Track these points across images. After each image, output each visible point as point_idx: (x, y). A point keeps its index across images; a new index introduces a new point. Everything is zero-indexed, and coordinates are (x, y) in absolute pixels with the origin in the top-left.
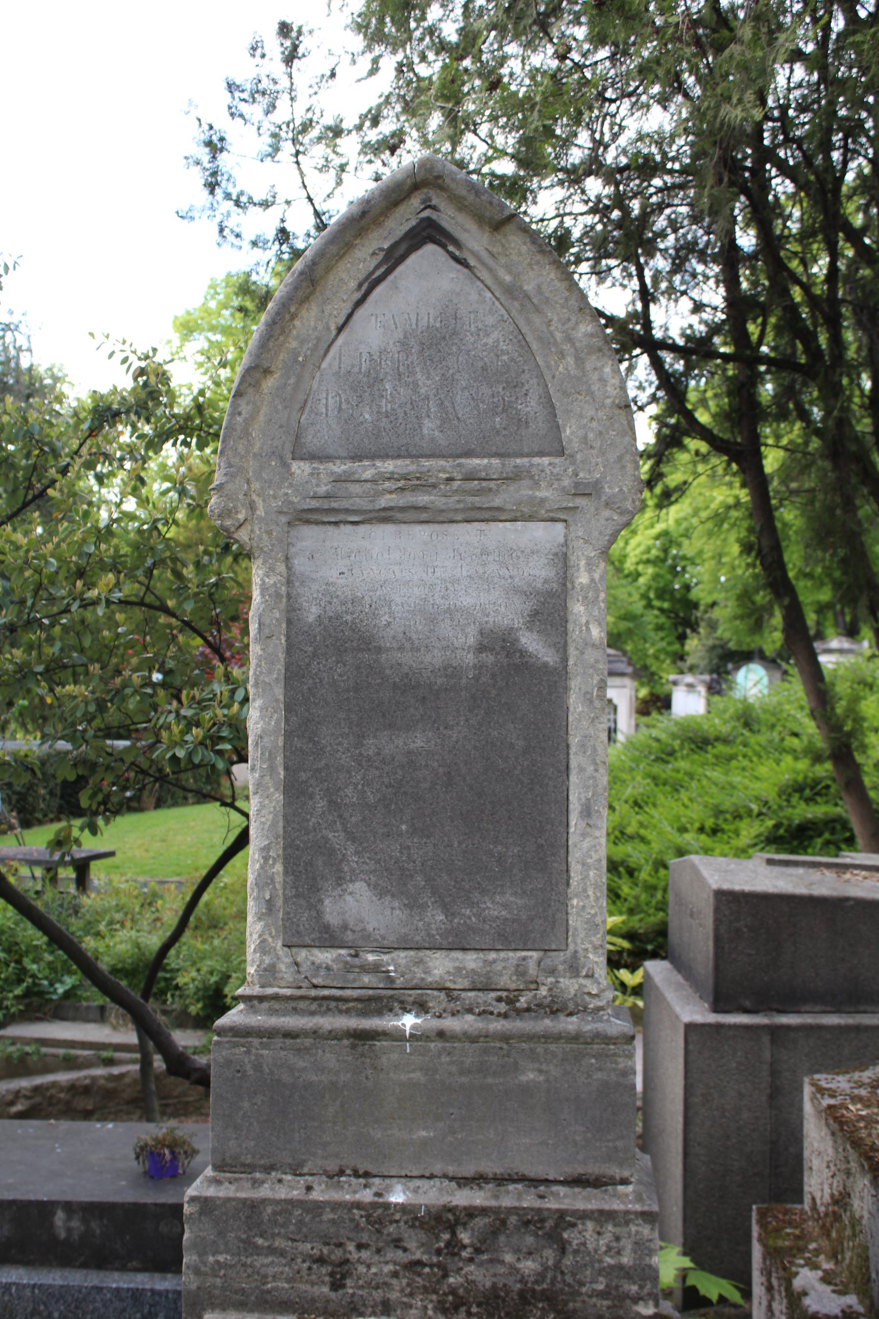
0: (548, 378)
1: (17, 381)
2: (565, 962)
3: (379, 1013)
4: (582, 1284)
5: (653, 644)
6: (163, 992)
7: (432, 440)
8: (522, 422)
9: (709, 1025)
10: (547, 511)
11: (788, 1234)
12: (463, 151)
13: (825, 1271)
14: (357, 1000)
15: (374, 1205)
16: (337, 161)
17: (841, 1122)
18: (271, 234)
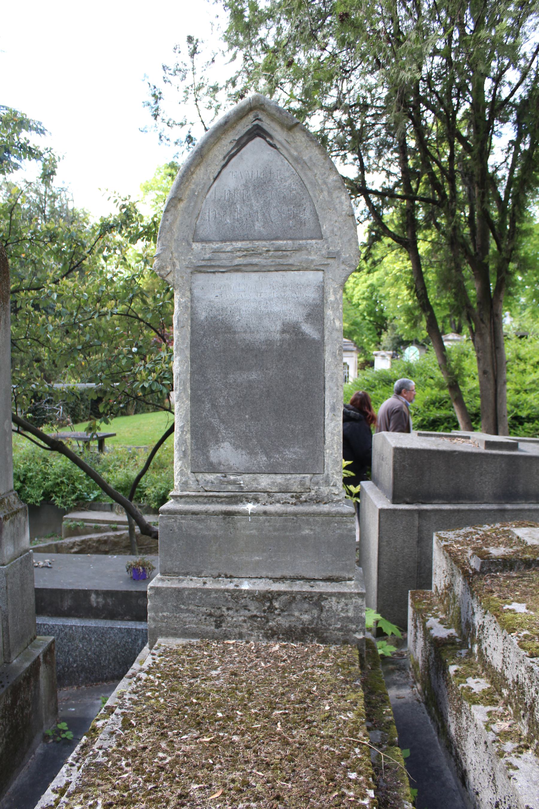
0: (315, 202)
1: (67, 215)
3: (236, 503)
4: (330, 625)
6: (139, 498)
7: (260, 232)
8: (302, 223)
12: (275, 97)
14: (226, 497)
15: (235, 591)
16: (215, 104)
18: (184, 138)
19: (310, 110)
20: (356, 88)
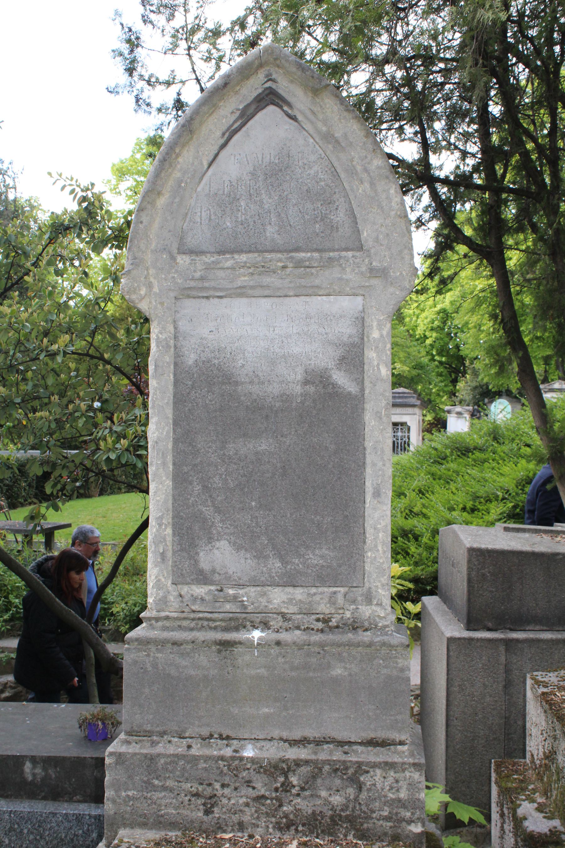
2: (362, 595)
3: (237, 629)
5: (436, 385)
7: (273, 240)
8: (334, 228)
9: (464, 639)
10: (351, 288)
11: (516, 779)
12: (301, 45)
13: (539, 803)
14: (221, 620)
15: (233, 758)
16: (215, 54)
17: (550, 703)
18: (170, 103)
19: (350, 63)
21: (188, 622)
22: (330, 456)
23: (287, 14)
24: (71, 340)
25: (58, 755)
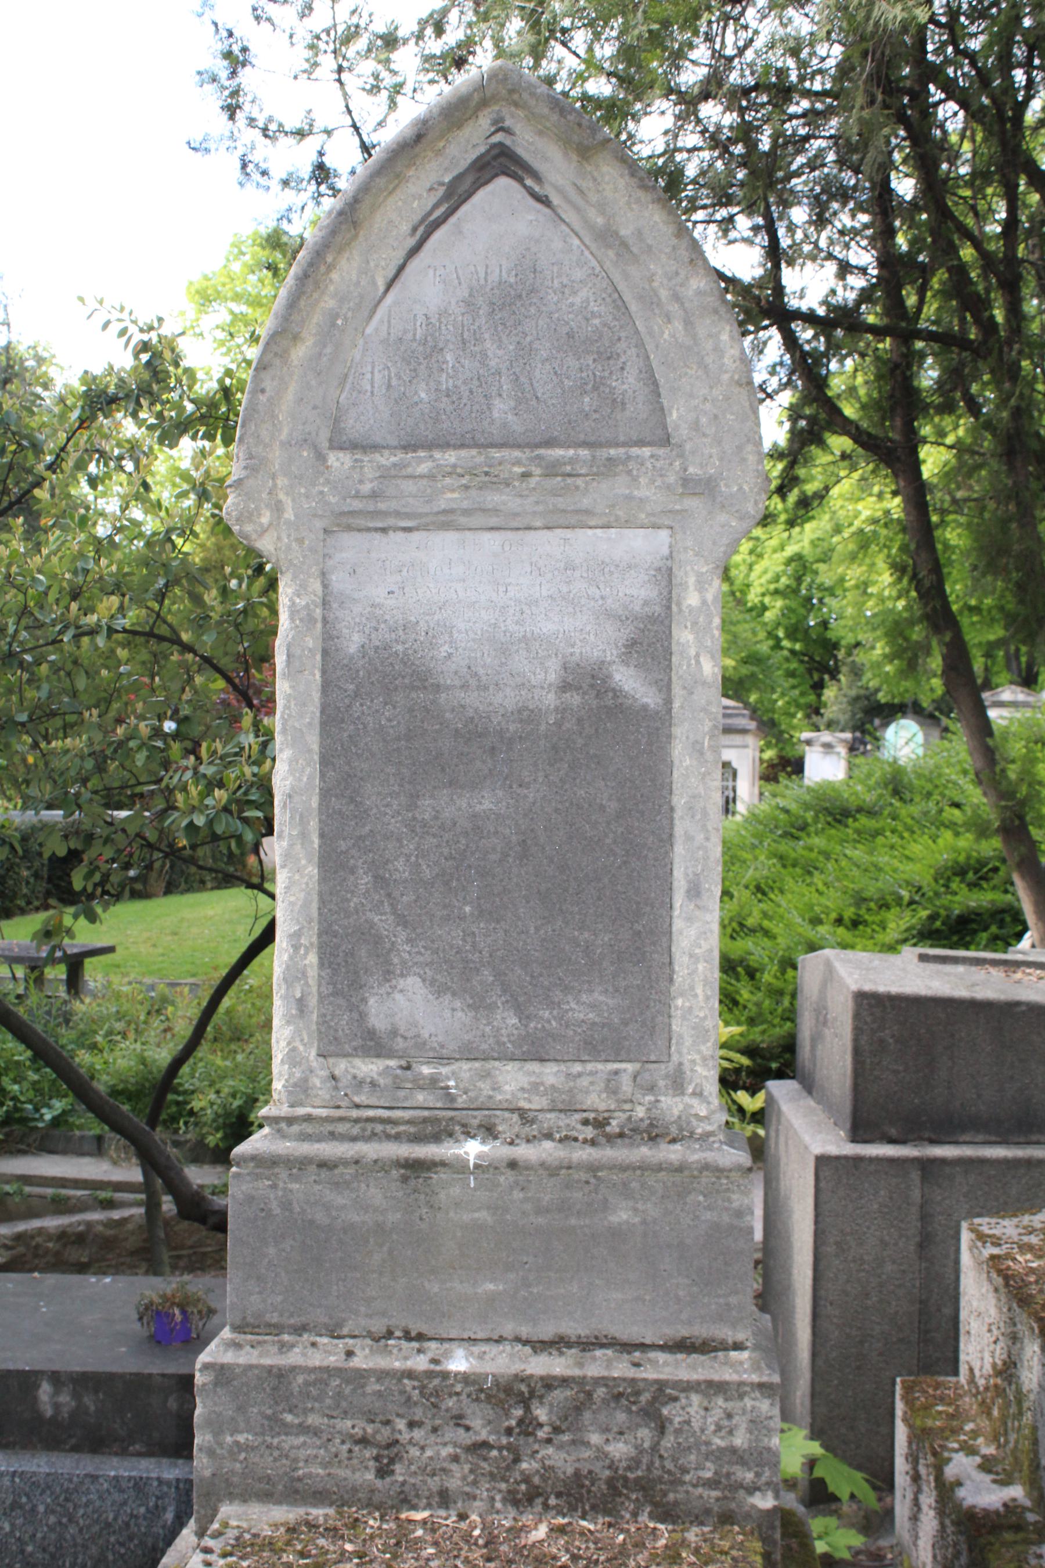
3: (436, 1138)
4: (685, 1471)
5: (783, 695)
6: (174, 1119)
7: (505, 425)
8: (617, 403)
12: (547, 67)
13: (983, 1457)
14: (409, 1122)
15: (430, 1374)
16: (388, 80)
19: (638, 98)
20: (759, 43)
21: (348, 1125)
22: (608, 823)
23: (523, 8)
24: (121, 608)
25: (101, 1369)
